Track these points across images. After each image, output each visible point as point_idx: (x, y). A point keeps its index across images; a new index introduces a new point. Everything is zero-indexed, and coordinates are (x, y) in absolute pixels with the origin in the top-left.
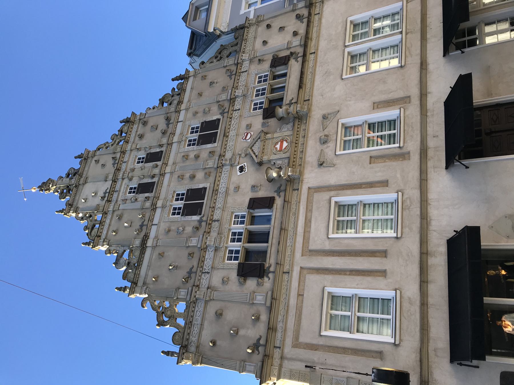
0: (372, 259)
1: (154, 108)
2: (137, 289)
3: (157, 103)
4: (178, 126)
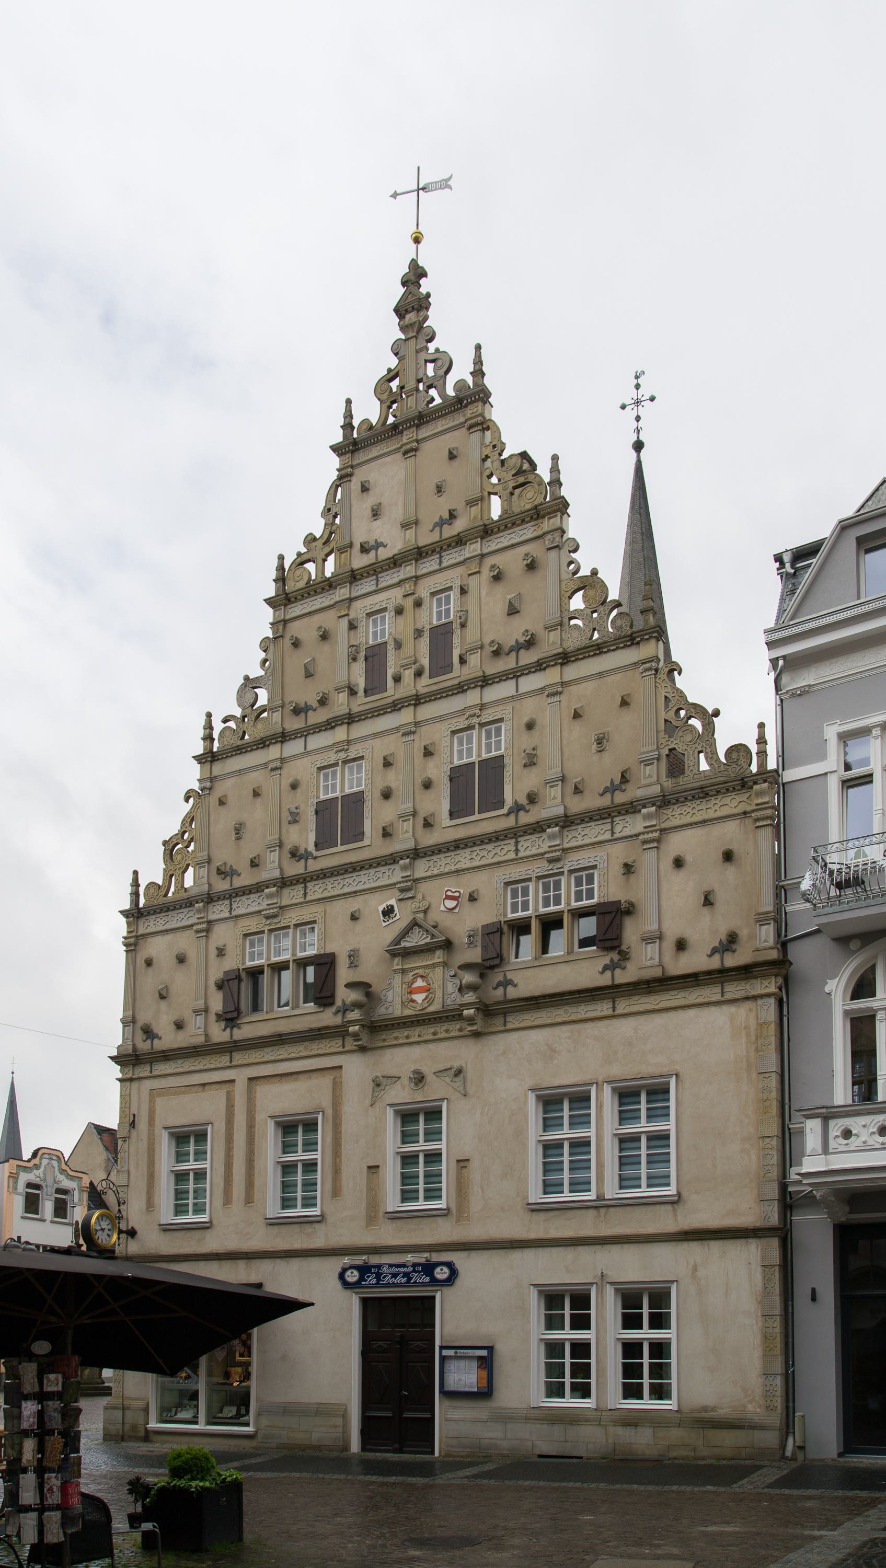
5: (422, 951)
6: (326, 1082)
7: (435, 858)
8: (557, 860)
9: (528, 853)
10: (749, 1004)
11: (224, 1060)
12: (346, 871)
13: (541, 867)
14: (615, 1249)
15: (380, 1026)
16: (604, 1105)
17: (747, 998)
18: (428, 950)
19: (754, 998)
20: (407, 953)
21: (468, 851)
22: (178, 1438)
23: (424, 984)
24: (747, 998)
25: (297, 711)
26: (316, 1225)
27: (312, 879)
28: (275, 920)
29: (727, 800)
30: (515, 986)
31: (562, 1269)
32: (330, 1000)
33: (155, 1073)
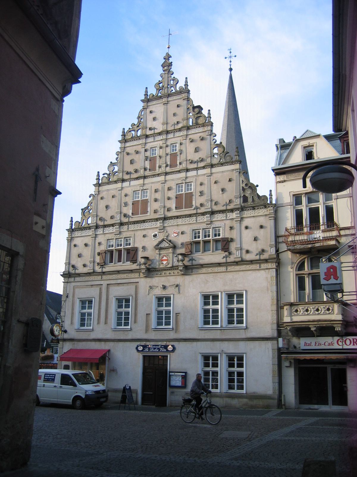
17: (267, 269)
23: (166, 258)
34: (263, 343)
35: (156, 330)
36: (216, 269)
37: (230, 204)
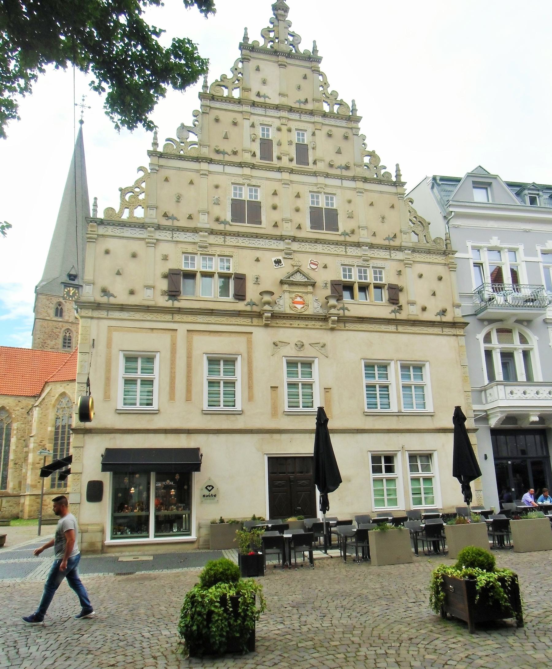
0: (184, 391)
1: (364, 144)
2: (156, 159)
3: (369, 149)
4: (337, 180)
5: (300, 285)
6: (243, 339)
7: (303, 244)
8: (367, 261)
9: (351, 254)
10: (455, 337)
11: (168, 317)
12: (252, 237)
13: (360, 262)
14: (408, 435)
15: (276, 316)
16: (394, 371)
17: (454, 335)
18: (305, 285)
19: (457, 335)
20: (292, 284)
21: (321, 245)
22: (147, 548)
23: (301, 300)
24: (454, 335)
25: (218, 152)
26: (238, 416)
27: (230, 235)
28: (205, 250)
29: (437, 257)
30: (349, 311)
31: (383, 444)
32: (243, 298)
33: (110, 316)
34: (442, 435)
35: (288, 414)
36: (383, 328)
37: (394, 239)
